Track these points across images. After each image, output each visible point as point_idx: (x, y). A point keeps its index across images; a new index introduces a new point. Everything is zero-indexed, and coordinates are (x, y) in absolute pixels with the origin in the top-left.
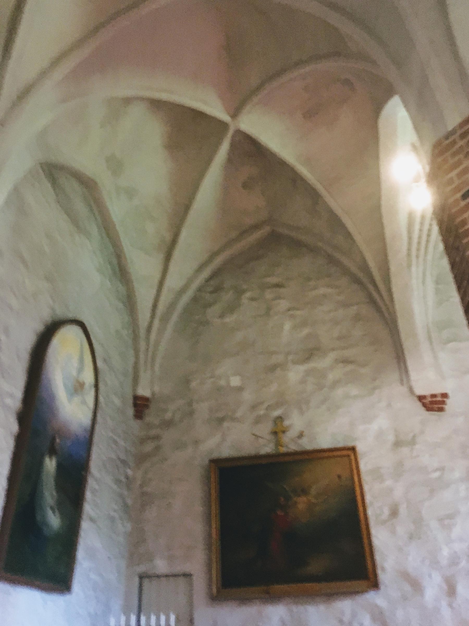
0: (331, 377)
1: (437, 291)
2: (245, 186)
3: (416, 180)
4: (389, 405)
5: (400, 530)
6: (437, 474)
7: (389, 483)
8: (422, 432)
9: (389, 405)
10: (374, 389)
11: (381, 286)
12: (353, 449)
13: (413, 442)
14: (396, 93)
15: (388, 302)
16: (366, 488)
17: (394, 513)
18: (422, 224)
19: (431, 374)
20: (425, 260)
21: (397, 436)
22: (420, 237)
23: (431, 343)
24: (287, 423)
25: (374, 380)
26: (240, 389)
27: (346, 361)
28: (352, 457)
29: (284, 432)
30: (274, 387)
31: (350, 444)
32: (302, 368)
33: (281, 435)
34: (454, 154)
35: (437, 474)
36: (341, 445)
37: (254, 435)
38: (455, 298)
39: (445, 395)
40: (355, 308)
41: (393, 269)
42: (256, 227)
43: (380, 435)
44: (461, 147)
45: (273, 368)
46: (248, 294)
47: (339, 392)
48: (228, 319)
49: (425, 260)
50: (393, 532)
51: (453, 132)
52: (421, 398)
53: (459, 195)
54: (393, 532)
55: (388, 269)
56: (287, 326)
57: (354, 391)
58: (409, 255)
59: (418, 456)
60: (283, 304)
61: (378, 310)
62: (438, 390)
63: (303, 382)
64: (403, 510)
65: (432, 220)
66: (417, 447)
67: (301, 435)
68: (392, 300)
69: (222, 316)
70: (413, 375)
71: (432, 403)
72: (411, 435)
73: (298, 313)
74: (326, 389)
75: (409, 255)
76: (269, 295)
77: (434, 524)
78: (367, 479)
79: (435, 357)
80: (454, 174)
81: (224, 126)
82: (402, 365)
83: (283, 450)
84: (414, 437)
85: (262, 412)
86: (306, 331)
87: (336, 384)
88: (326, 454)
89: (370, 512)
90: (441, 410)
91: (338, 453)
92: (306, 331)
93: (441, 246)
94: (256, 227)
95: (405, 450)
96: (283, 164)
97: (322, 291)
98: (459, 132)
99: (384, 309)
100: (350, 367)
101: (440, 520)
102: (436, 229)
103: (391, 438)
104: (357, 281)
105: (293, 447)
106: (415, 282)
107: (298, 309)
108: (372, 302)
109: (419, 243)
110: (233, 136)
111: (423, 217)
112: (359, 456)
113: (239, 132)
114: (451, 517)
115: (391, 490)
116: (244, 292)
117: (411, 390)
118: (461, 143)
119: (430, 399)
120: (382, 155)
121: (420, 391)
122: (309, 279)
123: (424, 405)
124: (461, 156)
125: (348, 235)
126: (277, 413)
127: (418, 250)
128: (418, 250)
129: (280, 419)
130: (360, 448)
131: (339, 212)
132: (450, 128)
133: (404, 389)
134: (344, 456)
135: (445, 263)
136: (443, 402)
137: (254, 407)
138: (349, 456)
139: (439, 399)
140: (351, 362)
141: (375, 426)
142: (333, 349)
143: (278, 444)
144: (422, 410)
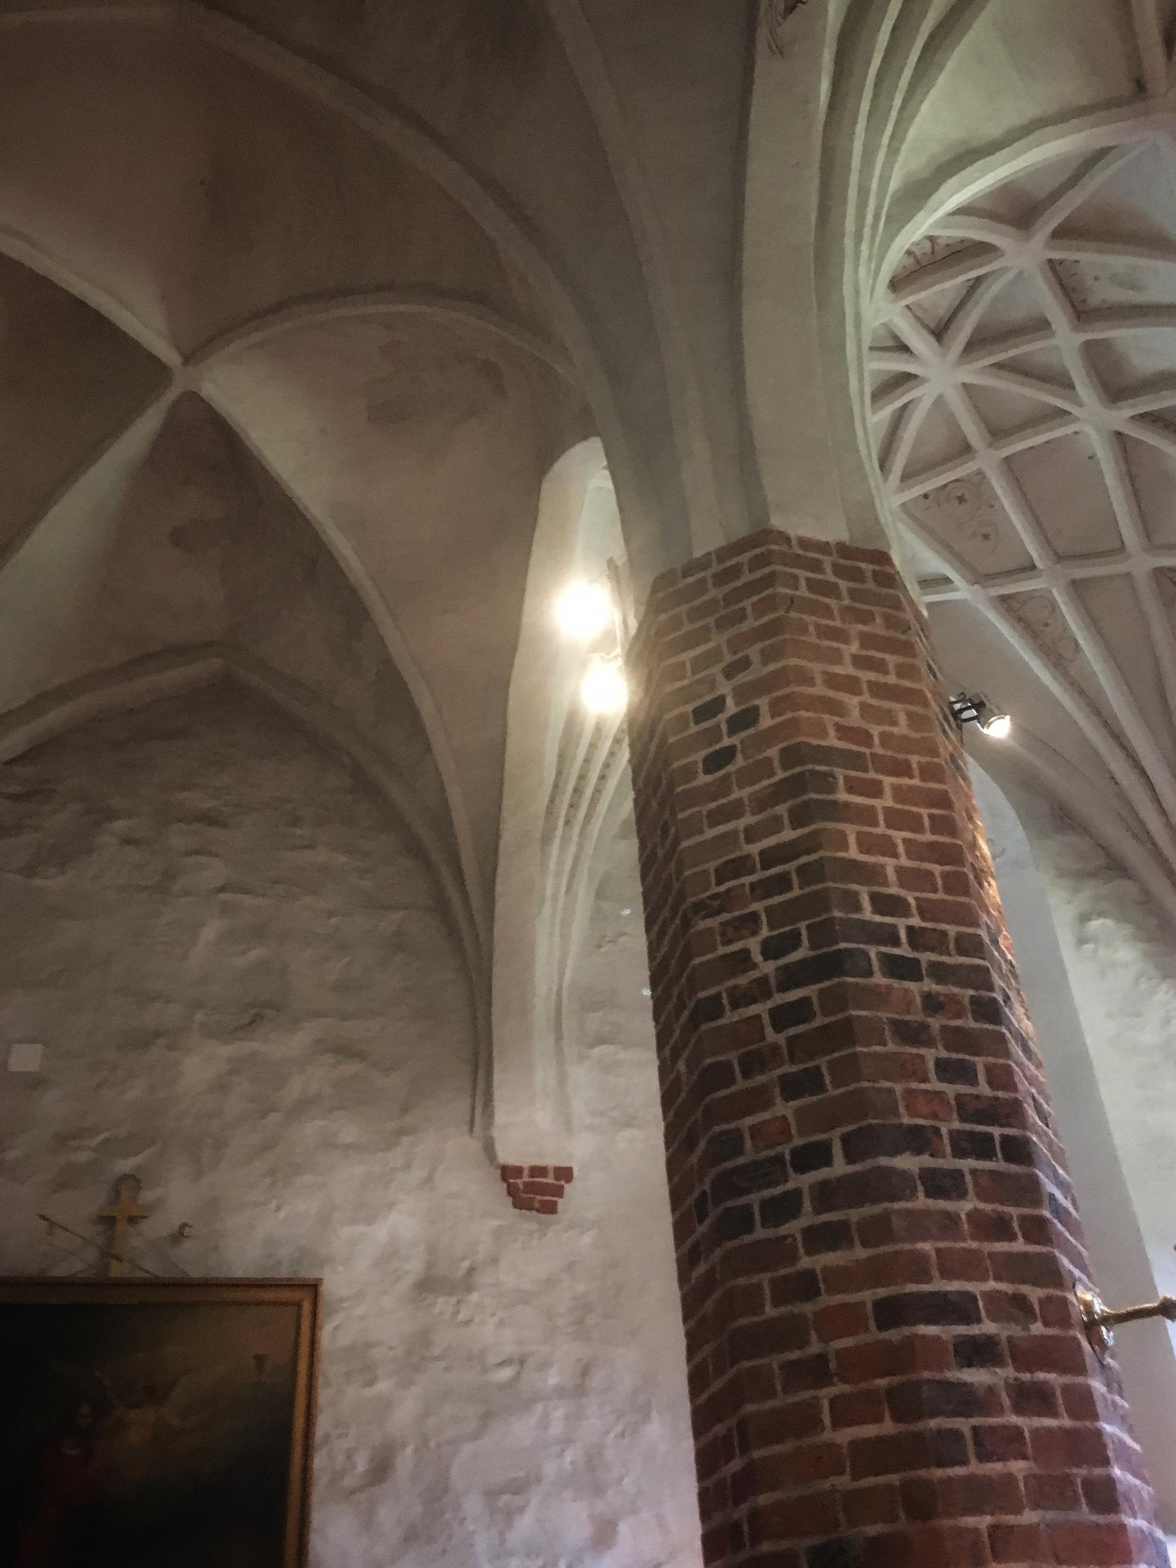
0: (295, 1087)
1: (597, 916)
2: (178, 538)
3: (602, 645)
4: (428, 1181)
5: (387, 1516)
6: (506, 1373)
7: (384, 1386)
8: (494, 1260)
9: (428, 1181)
10: (401, 1132)
11: (476, 904)
12: (313, 1287)
13: (466, 1283)
14: (597, 434)
15: (478, 918)
16: (323, 1396)
17: (381, 1470)
18: (593, 746)
19: (544, 1117)
20: (583, 833)
21: (430, 1265)
22: (582, 777)
23: (559, 1038)
24: (147, 1196)
25: (405, 1110)
26: (35, 1083)
27: (344, 1051)
28: (307, 1306)
29: (133, 1220)
30: (135, 1091)
31: (308, 1274)
32: (227, 1051)
33: (121, 1226)
34: (693, 616)
35: (506, 1373)
36: (284, 1273)
37: (43, 1217)
38: (637, 941)
39: (565, 1174)
40: (397, 916)
41: (507, 838)
42: (181, 652)
43: (390, 1256)
44: (713, 601)
45: (143, 1040)
46: (120, 825)
47: (311, 1128)
48: (51, 883)
49: (583, 833)
50: (368, 1522)
51: (703, 564)
52: (508, 1173)
53: (690, 708)
54: (368, 1522)
55: (497, 836)
56: (209, 933)
57: (349, 1132)
58: (550, 811)
59: (468, 1323)
60: (213, 872)
61: (453, 934)
62: (550, 1161)
63: (221, 1087)
64: (405, 1462)
65: (617, 741)
66: (474, 1297)
67: (180, 1235)
68: (490, 930)
69: (29, 870)
70: (502, 1114)
71: (529, 1187)
72: (466, 1264)
73: (246, 900)
74: (274, 1117)
75: (550, 811)
76: (178, 839)
77: (473, 1505)
78: (330, 1370)
79: (562, 1079)
80: (687, 656)
81: (159, 372)
82: (481, 1074)
83: (117, 1270)
84: (471, 1270)
85: (83, 1157)
86: (255, 954)
87: (305, 1106)
88: (240, 1295)
89: (319, 1461)
90: (551, 1208)
91: (269, 1295)
92: (255, 954)
93: (627, 807)
94: (181, 652)
95: (443, 1304)
96: (290, 510)
97: (322, 856)
98: (716, 568)
99: (468, 942)
100: (352, 1068)
101: (491, 1494)
102: (625, 755)
103: (414, 1267)
104: (415, 850)
105: (151, 1267)
106: (551, 884)
107: (245, 892)
108: (441, 908)
109: (578, 791)
110: (176, 404)
111: (598, 730)
112: (322, 1310)
113: (193, 398)
114: (518, 1487)
115: (386, 1405)
116: (112, 815)
117: (489, 1149)
118: (714, 593)
119: (526, 1179)
120: (538, 552)
121: (507, 1155)
122: (296, 822)
123: (512, 1191)
124: (711, 620)
125: (417, 729)
126: (125, 1165)
127: (573, 806)
128: (573, 806)
129: (133, 1182)
130: (335, 1284)
131: (408, 671)
132: (698, 553)
133: (474, 1145)
134: (285, 1304)
135: (629, 849)
136: (559, 1192)
137: (63, 1140)
138: (299, 1305)
139: (550, 1180)
140: (361, 1056)
141: (381, 1232)
142: (317, 1015)
143: (109, 1253)
144: (507, 1212)
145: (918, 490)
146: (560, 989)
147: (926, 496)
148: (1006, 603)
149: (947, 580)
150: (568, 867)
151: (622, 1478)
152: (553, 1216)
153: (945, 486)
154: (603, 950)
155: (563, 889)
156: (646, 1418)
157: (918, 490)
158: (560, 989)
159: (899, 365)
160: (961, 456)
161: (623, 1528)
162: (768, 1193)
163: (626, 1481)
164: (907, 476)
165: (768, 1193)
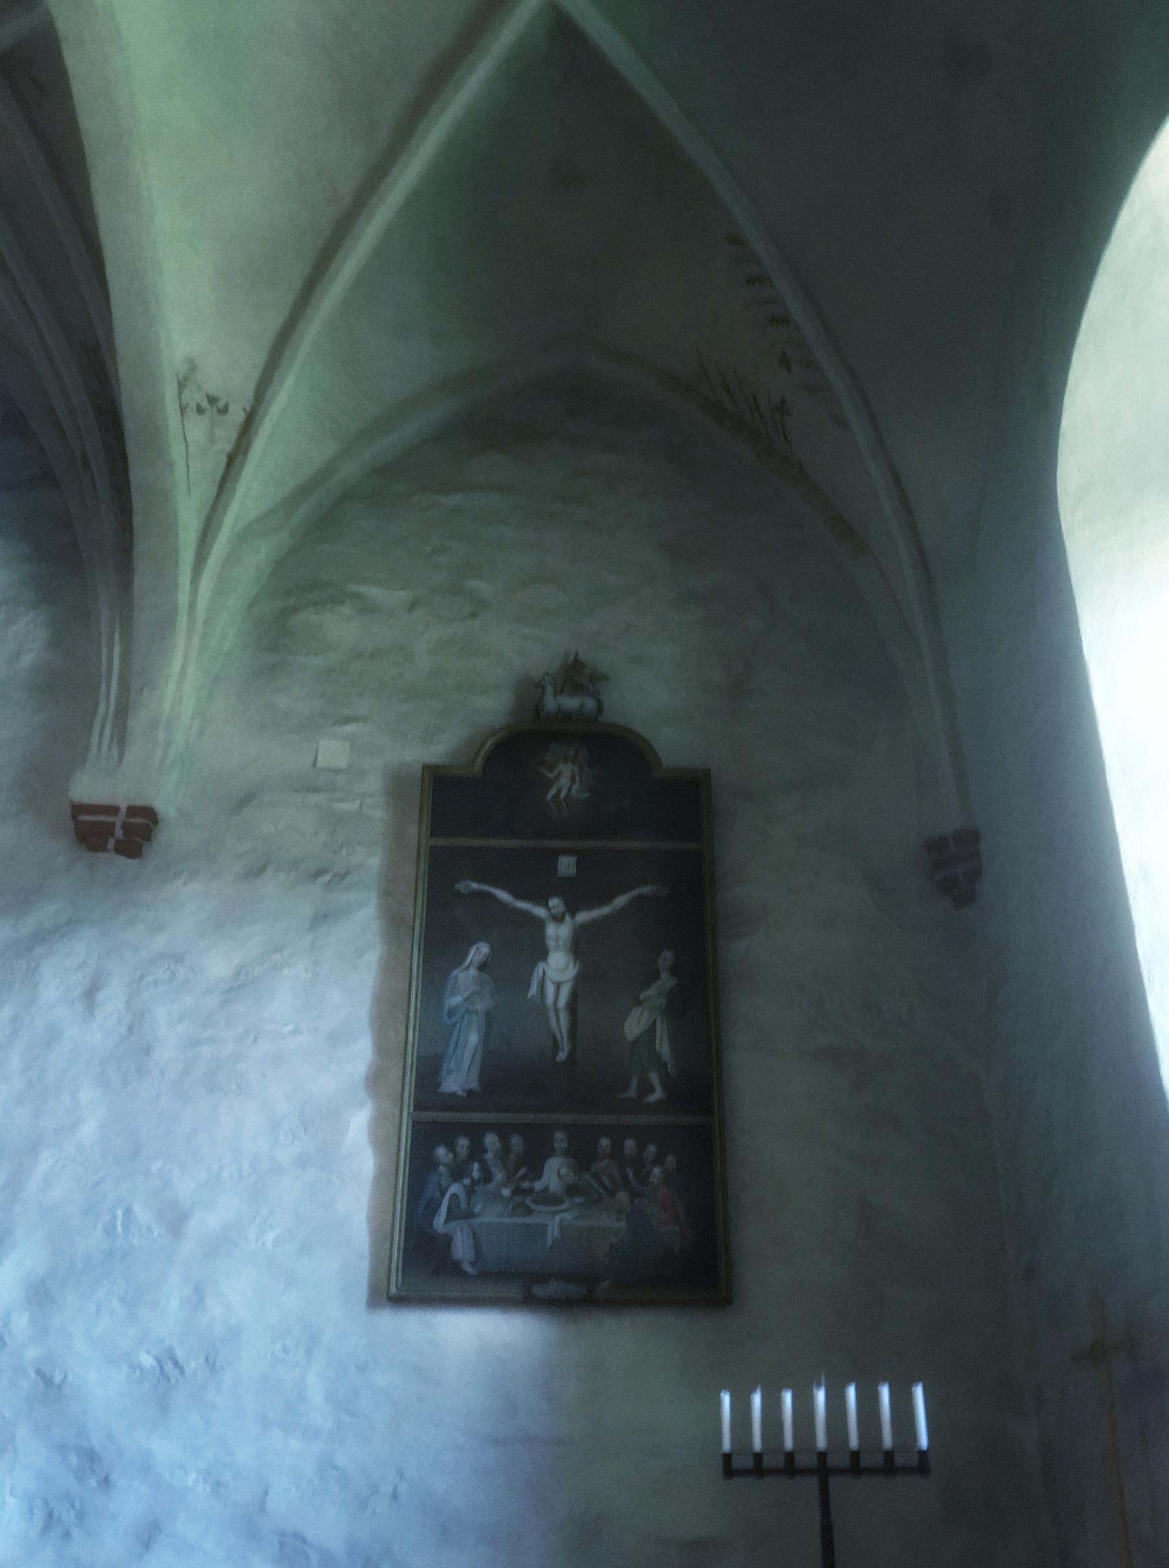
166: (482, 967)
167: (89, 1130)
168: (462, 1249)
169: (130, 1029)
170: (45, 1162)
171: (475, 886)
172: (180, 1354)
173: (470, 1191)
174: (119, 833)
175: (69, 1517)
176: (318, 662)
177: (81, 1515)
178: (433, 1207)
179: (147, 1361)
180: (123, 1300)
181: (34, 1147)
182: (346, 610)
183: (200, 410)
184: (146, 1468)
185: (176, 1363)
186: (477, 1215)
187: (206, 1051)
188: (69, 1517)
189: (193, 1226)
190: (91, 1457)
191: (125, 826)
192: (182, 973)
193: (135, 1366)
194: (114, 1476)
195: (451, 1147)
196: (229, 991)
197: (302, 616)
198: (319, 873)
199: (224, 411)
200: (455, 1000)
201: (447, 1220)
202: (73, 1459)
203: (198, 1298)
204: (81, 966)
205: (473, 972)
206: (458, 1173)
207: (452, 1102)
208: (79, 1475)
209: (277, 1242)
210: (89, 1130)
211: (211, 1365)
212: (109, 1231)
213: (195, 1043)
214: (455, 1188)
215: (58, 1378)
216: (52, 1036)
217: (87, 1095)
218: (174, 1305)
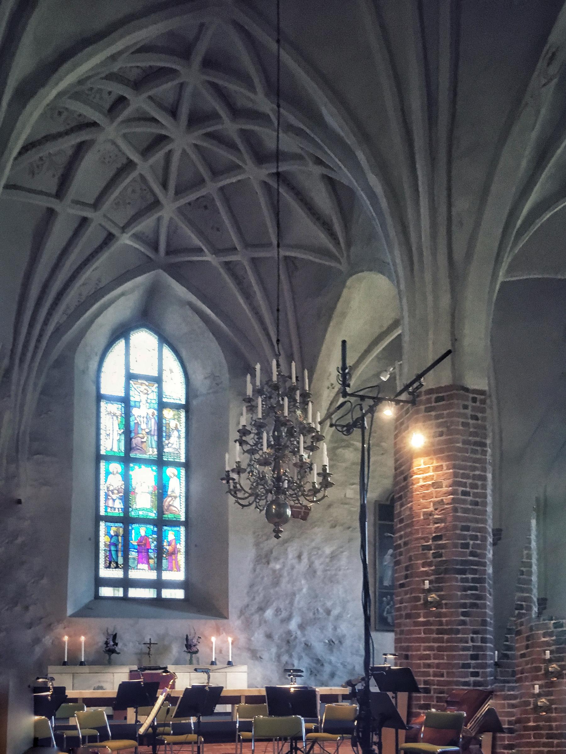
145: (183, 201)
146: (19, 433)
147: (189, 204)
148: (227, 264)
149: (201, 250)
150: (22, 382)
151: (32, 595)
152: (225, 621)
153: (198, 199)
154: (42, 417)
155: (20, 391)
156: (42, 578)
157: (183, 201)
158: (19, 433)
159: (155, 130)
160: (21, 187)
161: (31, 608)
162: (441, 661)
163: (33, 596)
164: (179, 192)
165: (441, 661)
166: (391, 555)
167: (305, 590)
168: (390, 620)
169: (310, 566)
170: (297, 598)
171: (389, 534)
172: (334, 640)
173: (391, 607)
174: (302, 514)
175: (315, 672)
176: (344, 465)
177: (318, 672)
178: (384, 611)
179: (327, 641)
180: (320, 629)
181: (294, 594)
182: (351, 449)
183: (328, 388)
184: (330, 663)
185: (333, 642)
186: (392, 613)
187: (329, 573)
188: (315, 672)
189: (332, 613)
190: (318, 660)
191: (304, 512)
192: (320, 552)
193: (325, 642)
194: (324, 664)
195: (387, 598)
196: (331, 558)
197: (340, 450)
198: (349, 528)
199: (333, 388)
200: (385, 563)
201: (387, 614)
202: (315, 661)
203: (335, 629)
204: (296, 550)
205: (389, 556)
206: (388, 604)
207: (386, 587)
208: (316, 664)
209: (350, 617)
210: (305, 590)
211: (340, 642)
212: (314, 614)
213: (326, 570)
214: (388, 607)
215: (309, 644)
216: (293, 568)
217: (303, 582)
218: (330, 630)
